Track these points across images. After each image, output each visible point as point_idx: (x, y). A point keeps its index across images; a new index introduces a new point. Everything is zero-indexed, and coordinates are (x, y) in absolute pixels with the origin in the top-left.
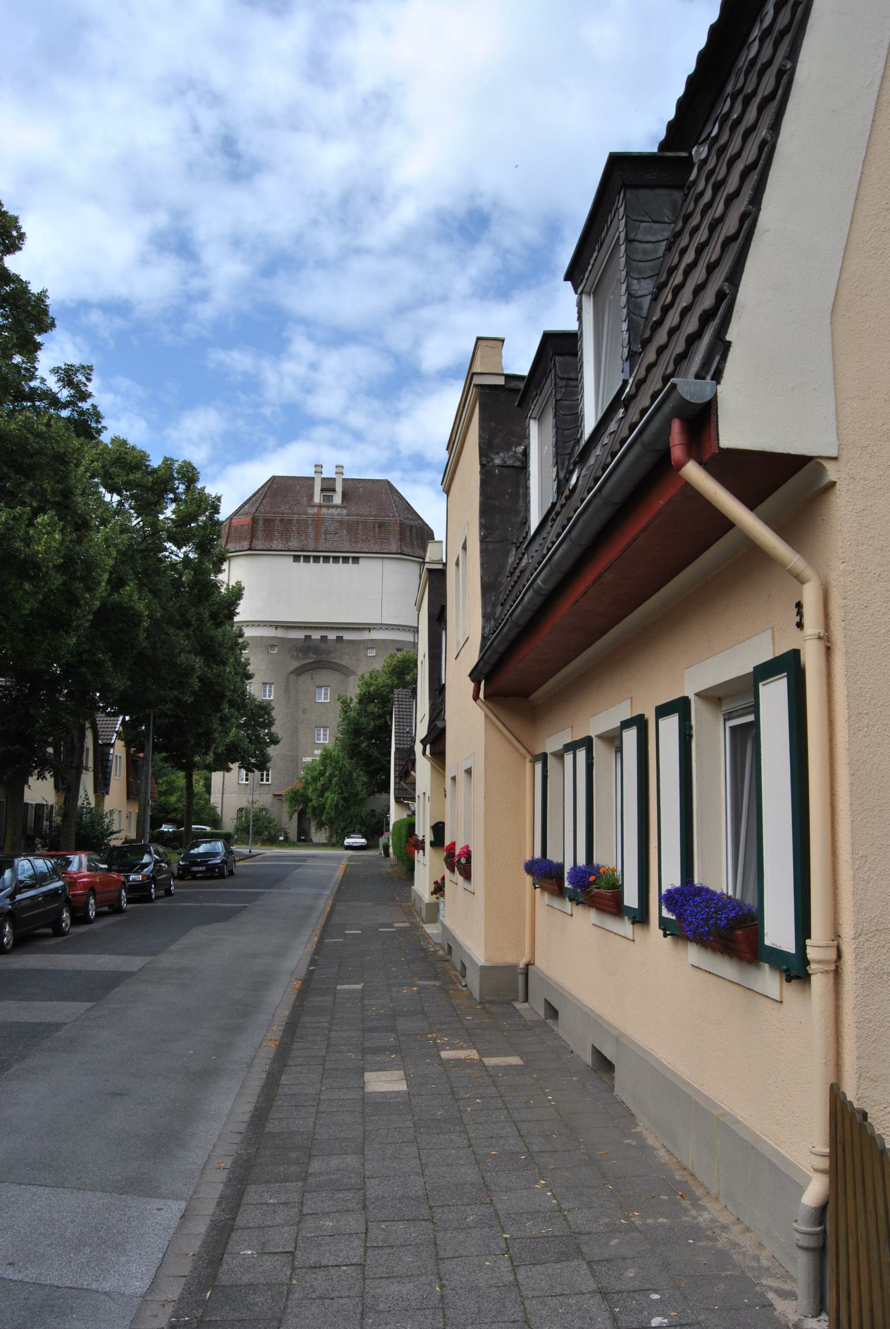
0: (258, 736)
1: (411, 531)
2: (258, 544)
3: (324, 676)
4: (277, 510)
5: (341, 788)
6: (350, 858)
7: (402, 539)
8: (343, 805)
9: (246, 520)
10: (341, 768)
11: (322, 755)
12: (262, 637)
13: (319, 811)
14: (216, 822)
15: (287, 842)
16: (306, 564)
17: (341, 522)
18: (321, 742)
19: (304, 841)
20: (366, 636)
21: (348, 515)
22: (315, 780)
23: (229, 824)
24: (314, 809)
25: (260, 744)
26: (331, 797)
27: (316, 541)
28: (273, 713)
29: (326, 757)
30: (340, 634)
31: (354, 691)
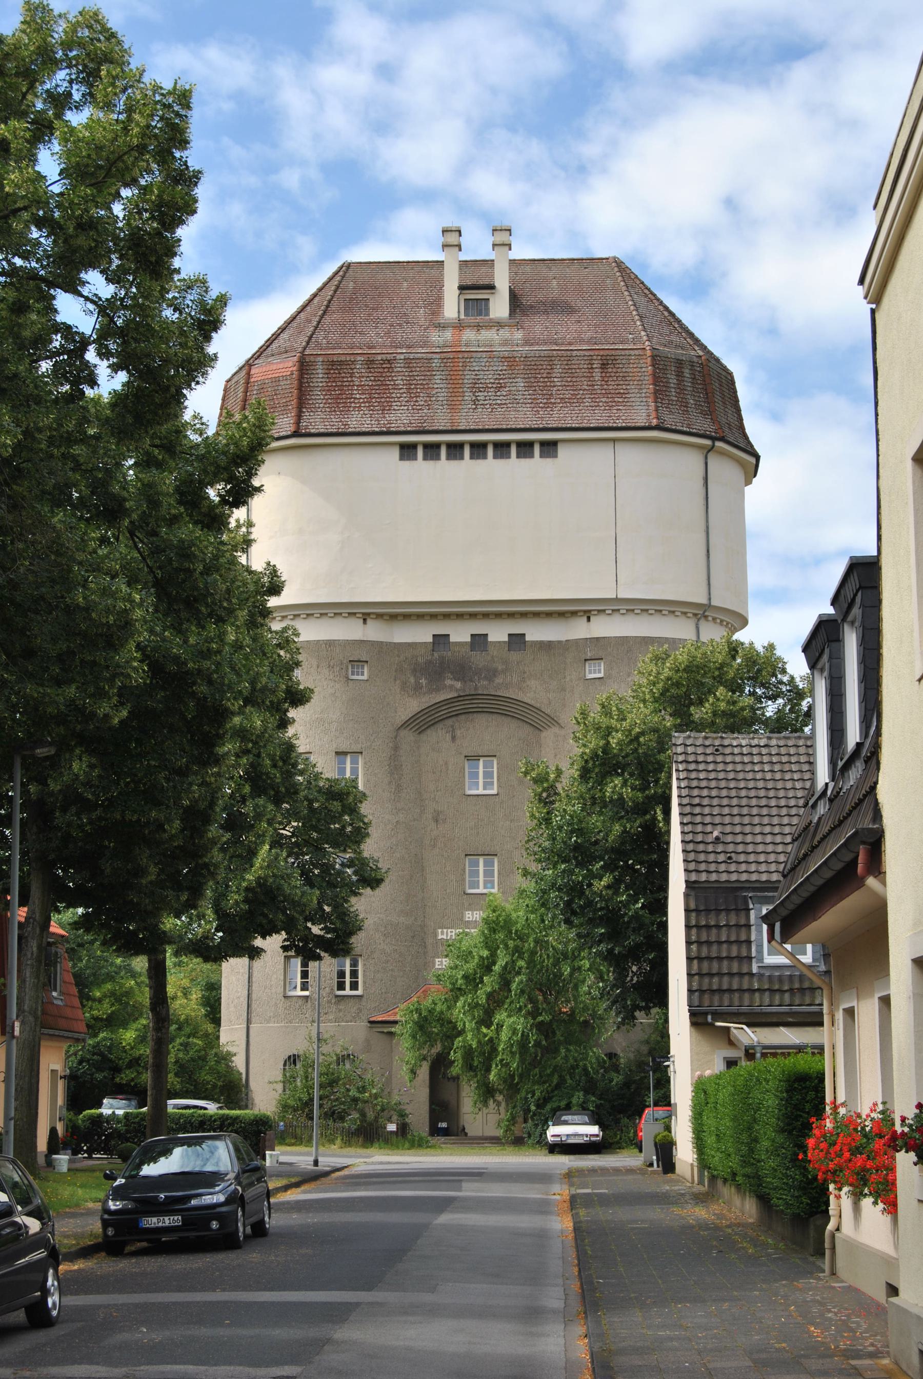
0: (327, 868)
1: (680, 374)
2: (315, 421)
3: (483, 731)
4: (358, 339)
5: (531, 1000)
6: (570, 1176)
7: (659, 394)
8: (537, 1044)
9: (286, 366)
10: (533, 953)
11: (486, 921)
12: (330, 643)
13: (481, 1059)
14: (232, 1090)
15: (404, 1136)
16: (431, 464)
17: (510, 360)
18: (481, 890)
19: (446, 1132)
20: (579, 630)
21: (527, 342)
22: (473, 981)
23: (265, 1097)
24: (468, 1053)
25: (337, 888)
26: (510, 1024)
27: (453, 407)
28: (365, 808)
29: (498, 927)
30: (517, 628)
31: (564, 754)
